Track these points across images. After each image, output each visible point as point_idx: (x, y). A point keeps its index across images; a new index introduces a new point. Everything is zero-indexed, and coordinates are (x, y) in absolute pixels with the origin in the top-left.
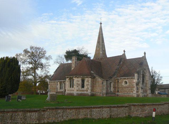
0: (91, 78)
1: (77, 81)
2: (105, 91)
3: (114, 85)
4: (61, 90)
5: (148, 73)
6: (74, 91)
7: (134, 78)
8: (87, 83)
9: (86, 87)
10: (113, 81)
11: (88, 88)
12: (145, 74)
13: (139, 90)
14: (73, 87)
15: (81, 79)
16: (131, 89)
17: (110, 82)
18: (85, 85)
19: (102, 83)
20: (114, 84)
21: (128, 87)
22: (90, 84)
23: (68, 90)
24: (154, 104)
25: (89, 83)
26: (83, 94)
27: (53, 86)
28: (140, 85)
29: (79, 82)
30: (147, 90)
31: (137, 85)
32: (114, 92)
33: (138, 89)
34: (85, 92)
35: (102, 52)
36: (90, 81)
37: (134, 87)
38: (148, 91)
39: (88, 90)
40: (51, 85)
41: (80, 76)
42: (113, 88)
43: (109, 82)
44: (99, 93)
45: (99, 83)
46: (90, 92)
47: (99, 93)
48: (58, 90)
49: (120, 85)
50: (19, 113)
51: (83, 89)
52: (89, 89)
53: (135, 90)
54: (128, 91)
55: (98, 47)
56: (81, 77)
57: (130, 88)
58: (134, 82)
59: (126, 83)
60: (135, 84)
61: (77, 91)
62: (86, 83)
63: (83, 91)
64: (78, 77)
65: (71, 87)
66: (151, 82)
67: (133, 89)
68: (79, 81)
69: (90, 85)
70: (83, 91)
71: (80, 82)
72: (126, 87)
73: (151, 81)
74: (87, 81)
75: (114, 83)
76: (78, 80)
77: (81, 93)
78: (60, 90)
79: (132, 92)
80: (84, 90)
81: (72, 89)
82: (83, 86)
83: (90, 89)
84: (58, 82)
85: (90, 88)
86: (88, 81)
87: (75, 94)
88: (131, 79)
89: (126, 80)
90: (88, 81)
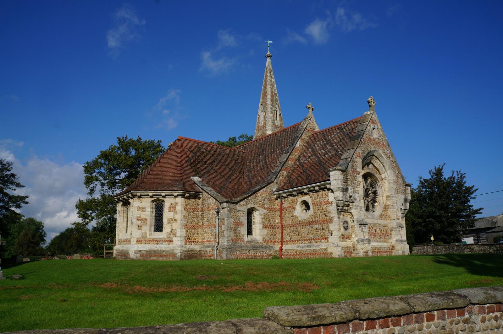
0: (183, 195)
1: (139, 208)
2: (224, 242)
3: (265, 218)
5: (388, 172)
10: (264, 204)
11: (173, 232)
12: (377, 176)
13: (350, 230)
15: (153, 201)
16: (323, 229)
17: (250, 206)
18: (165, 221)
19: (218, 212)
20: (265, 214)
21: (311, 223)
22: (178, 217)
24: (364, 308)
25: (176, 213)
26: (155, 251)
28: (353, 211)
29: (143, 213)
30: (392, 230)
31: (343, 211)
32: (270, 244)
33: (346, 228)
34: (164, 247)
36: (179, 208)
37: (331, 221)
38: (393, 233)
41: (146, 193)
42: (265, 227)
43: (242, 209)
46: (182, 246)
47: (209, 249)
48: (148, 237)
49: (286, 215)
51: (158, 235)
52: (175, 234)
53: (334, 233)
54: (311, 236)
56: (151, 194)
57: (317, 226)
58: (330, 201)
60: (333, 209)
61: (139, 241)
62: (167, 215)
63: (157, 241)
64: (139, 194)
66: (406, 200)
67: (328, 228)
68: (143, 209)
69: (179, 222)
70: (157, 241)
73: (402, 197)
74: (170, 208)
75: (266, 211)
76: (142, 205)
77: (150, 251)
79: (326, 238)
82: (159, 227)
83: (179, 233)
86: (173, 208)
87: (132, 255)
88: (321, 193)
89: (306, 198)
90: (175, 207)
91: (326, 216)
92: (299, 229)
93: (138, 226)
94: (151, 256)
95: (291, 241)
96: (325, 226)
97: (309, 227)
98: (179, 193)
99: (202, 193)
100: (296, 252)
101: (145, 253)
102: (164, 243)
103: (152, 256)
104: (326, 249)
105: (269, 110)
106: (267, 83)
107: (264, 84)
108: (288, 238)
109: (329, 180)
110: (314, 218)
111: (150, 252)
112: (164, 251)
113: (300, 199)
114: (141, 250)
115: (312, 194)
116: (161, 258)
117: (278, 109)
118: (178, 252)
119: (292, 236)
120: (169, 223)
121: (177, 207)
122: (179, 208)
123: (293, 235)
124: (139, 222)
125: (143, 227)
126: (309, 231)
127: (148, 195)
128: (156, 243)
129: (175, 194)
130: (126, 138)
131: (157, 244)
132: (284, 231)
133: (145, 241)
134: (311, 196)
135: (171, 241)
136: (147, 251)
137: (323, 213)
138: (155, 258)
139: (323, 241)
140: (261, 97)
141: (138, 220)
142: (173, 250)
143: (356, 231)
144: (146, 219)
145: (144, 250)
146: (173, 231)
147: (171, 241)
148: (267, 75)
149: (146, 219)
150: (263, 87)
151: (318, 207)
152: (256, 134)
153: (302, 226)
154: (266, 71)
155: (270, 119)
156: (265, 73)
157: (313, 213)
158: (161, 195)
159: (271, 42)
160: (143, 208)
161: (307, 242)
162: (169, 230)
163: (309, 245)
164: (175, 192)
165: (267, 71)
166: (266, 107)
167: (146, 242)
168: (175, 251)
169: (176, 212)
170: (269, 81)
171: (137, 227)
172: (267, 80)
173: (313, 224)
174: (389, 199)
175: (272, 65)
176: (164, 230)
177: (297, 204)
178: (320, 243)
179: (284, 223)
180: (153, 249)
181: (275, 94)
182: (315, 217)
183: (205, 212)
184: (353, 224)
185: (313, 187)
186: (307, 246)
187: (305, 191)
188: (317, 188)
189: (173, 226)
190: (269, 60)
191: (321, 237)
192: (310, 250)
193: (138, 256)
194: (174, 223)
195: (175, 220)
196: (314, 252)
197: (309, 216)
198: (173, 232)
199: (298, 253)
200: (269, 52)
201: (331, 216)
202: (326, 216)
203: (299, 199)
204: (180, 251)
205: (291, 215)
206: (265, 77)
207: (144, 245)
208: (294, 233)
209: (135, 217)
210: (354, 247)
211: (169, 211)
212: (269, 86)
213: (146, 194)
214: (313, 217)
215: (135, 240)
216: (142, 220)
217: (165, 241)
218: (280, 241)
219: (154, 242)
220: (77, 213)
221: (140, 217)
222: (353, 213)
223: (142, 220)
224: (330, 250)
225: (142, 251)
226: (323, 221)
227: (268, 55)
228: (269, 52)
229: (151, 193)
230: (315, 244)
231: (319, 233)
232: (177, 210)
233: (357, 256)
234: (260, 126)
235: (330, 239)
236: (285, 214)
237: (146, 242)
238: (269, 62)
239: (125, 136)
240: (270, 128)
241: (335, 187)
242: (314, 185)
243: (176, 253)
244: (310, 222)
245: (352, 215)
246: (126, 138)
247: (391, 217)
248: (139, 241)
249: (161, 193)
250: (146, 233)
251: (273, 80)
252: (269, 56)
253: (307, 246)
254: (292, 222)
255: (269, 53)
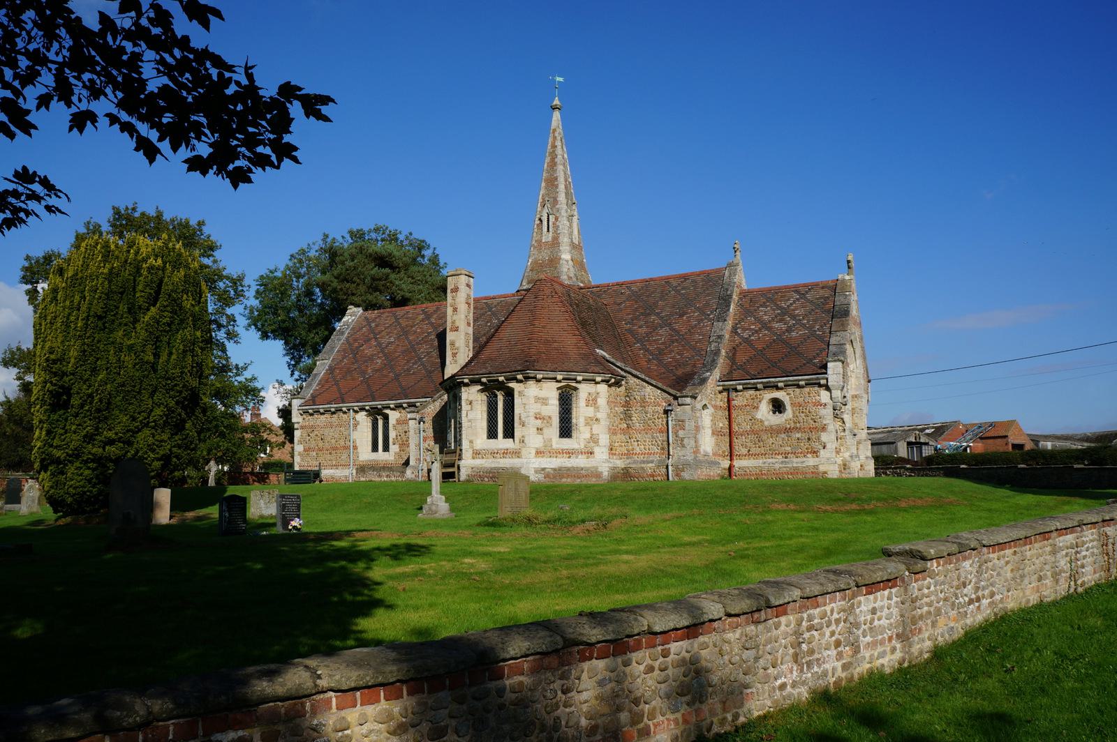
1: (537, 399)
4: (381, 455)
5: (858, 362)
6: (517, 454)
7: (823, 382)
8: (590, 411)
9: (578, 440)
11: (594, 439)
14: (509, 433)
15: (558, 389)
21: (787, 431)
22: (602, 415)
23: (477, 454)
25: (597, 408)
26: (568, 469)
27: (326, 431)
29: (544, 407)
34: (581, 462)
35: (570, 252)
36: (602, 401)
37: (824, 429)
39: (597, 450)
40: (313, 428)
41: (551, 375)
44: (652, 462)
45: (650, 409)
47: (650, 465)
50: (828, 608)
51: (566, 443)
53: (828, 446)
54: (788, 449)
55: (545, 229)
57: (798, 435)
58: (823, 401)
59: (778, 406)
61: (539, 453)
62: (581, 411)
63: (570, 453)
65: (492, 434)
67: (819, 438)
68: (544, 401)
70: (570, 453)
71: (553, 409)
72: (775, 431)
74: (588, 400)
76: (543, 394)
77: (560, 469)
78: (374, 456)
80: (576, 446)
81: (501, 443)
82: (566, 430)
84: (362, 409)
85: (604, 439)
86: (592, 401)
88: (807, 390)
90: (595, 400)
91: (815, 422)
92: (765, 437)
93: (538, 429)
94: (562, 477)
95: (750, 454)
96: (813, 436)
97: (783, 436)
98: (605, 377)
99: (625, 377)
100: (761, 471)
101: (552, 472)
102: (580, 456)
103: (563, 477)
104: (816, 467)
105: (563, 213)
106: (556, 160)
107: (548, 160)
108: (744, 451)
109: (826, 373)
110: (793, 424)
111: (559, 470)
112: (582, 469)
113: (768, 395)
114: (545, 468)
115: (790, 390)
116: (579, 480)
117: (576, 213)
118: (605, 470)
119: (750, 447)
120: (587, 424)
121: (599, 400)
122: (602, 401)
123: (754, 446)
124: (539, 422)
125: (545, 430)
126: (784, 442)
127: (555, 378)
128: (568, 455)
129: (598, 379)
130: (134, 209)
131: (570, 457)
132: (736, 440)
133: (550, 452)
134: (788, 392)
135: (591, 453)
136: (555, 470)
137: (810, 418)
138: (569, 480)
139: (809, 455)
140: (543, 184)
141: (536, 418)
142: (597, 468)
143: (848, 443)
144: (550, 417)
145: (552, 467)
146: (594, 437)
147: (591, 453)
148: (556, 144)
149: (550, 417)
150: (546, 165)
151: (801, 408)
152: (534, 254)
153: (771, 434)
154: (551, 135)
155: (566, 232)
156: (550, 140)
157: (791, 416)
158: (575, 379)
159: (561, 79)
160: (543, 399)
161: (780, 457)
162: (588, 435)
163: (785, 462)
164: (600, 376)
165: (555, 138)
166: (557, 207)
167: (551, 454)
168: (600, 469)
169: (598, 408)
170: (559, 157)
171: (535, 429)
172: (556, 155)
173: (791, 432)
174: (856, 399)
175: (562, 126)
176: (574, 434)
177: (762, 402)
178: (805, 459)
179: (735, 428)
180: (564, 465)
181: (569, 182)
182: (795, 423)
183: (634, 409)
184: (842, 434)
185: (796, 380)
186: (782, 462)
187: (780, 385)
188: (802, 383)
189: (593, 430)
190: (557, 115)
191: (806, 451)
192: (788, 467)
193: (541, 477)
194: (595, 425)
195: (597, 420)
196: (796, 471)
197: (784, 420)
198: (594, 439)
199: (766, 472)
200: (557, 98)
201: (824, 422)
202: (815, 422)
203: (765, 395)
204: (608, 469)
205: (750, 418)
206: (549, 147)
207: (549, 459)
208: (755, 444)
209: (532, 414)
210: (845, 465)
211: (587, 406)
212: (561, 167)
213: (551, 376)
214: (792, 421)
215: (533, 452)
216: (544, 419)
217: (582, 454)
218: (726, 454)
219: (565, 455)
220: (15, 377)
221: (539, 414)
222: (845, 420)
223: (544, 419)
224: (822, 468)
225: (547, 470)
226: (810, 428)
227: (556, 105)
228: (557, 98)
229: (561, 374)
230: (795, 460)
231: (802, 444)
232: (598, 404)
233: (850, 476)
234: (543, 241)
235: (822, 452)
236: (737, 416)
237: (551, 454)
238: (558, 120)
239: (130, 207)
240: (568, 248)
241: (835, 383)
242: (800, 378)
243: (602, 472)
244: (786, 428)
245: (844, 422)
246: (134, 209)
247: (859, 425)
248: (539, 453)
249: (576, 375)
250: (551, 439)
251: (566, 156)
252: (558, 108)
253: (782, 462)
254: (751, 428)
255: (556, 102)
